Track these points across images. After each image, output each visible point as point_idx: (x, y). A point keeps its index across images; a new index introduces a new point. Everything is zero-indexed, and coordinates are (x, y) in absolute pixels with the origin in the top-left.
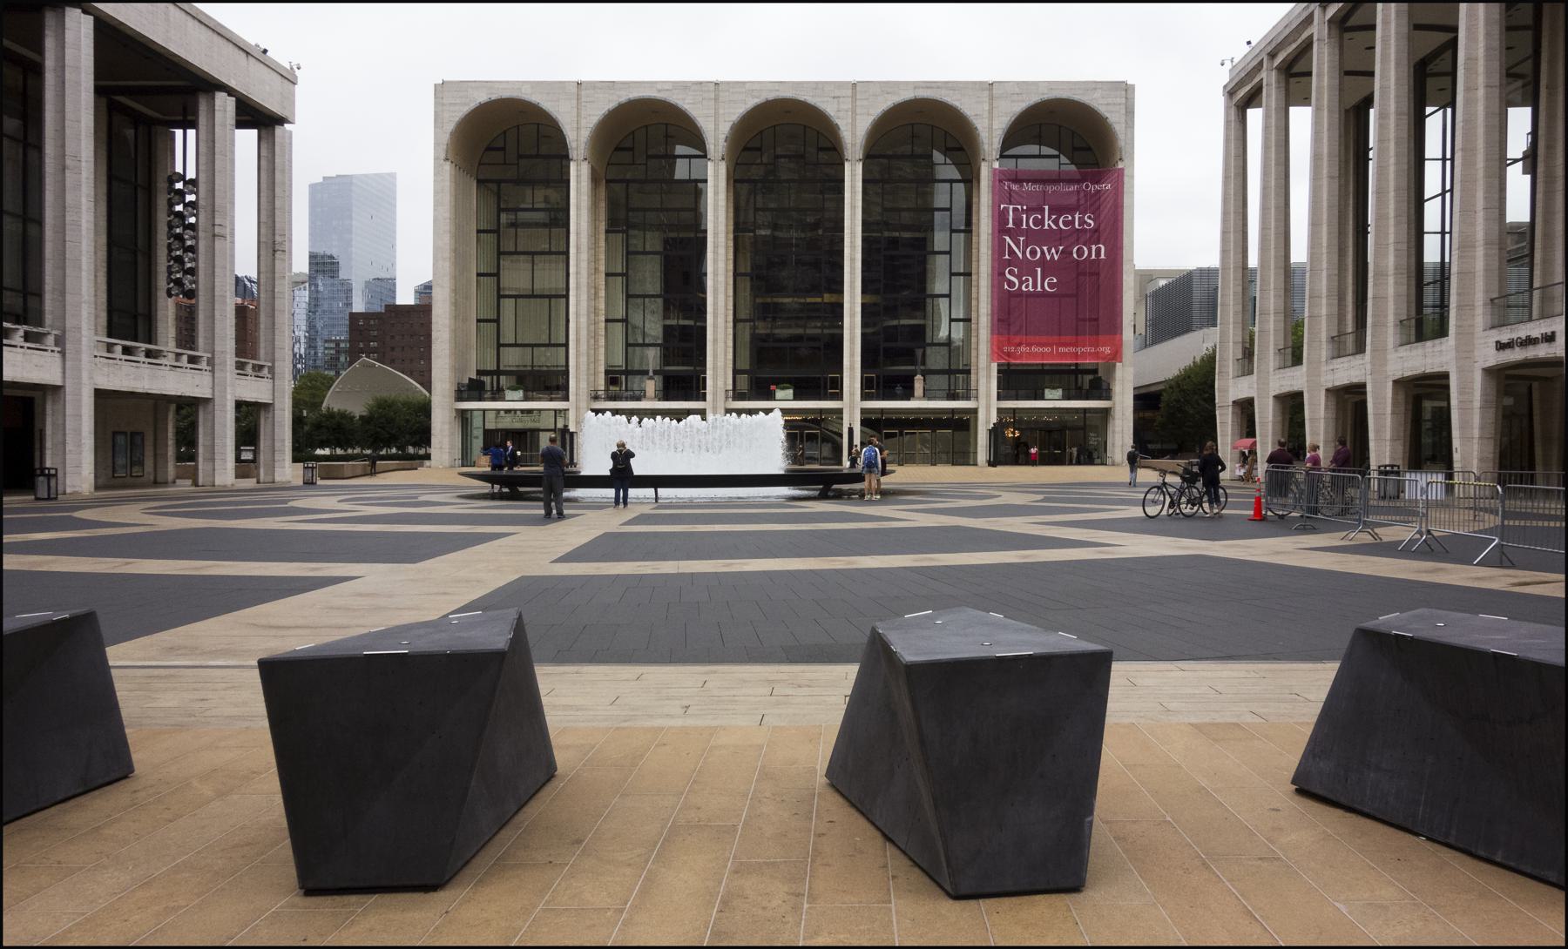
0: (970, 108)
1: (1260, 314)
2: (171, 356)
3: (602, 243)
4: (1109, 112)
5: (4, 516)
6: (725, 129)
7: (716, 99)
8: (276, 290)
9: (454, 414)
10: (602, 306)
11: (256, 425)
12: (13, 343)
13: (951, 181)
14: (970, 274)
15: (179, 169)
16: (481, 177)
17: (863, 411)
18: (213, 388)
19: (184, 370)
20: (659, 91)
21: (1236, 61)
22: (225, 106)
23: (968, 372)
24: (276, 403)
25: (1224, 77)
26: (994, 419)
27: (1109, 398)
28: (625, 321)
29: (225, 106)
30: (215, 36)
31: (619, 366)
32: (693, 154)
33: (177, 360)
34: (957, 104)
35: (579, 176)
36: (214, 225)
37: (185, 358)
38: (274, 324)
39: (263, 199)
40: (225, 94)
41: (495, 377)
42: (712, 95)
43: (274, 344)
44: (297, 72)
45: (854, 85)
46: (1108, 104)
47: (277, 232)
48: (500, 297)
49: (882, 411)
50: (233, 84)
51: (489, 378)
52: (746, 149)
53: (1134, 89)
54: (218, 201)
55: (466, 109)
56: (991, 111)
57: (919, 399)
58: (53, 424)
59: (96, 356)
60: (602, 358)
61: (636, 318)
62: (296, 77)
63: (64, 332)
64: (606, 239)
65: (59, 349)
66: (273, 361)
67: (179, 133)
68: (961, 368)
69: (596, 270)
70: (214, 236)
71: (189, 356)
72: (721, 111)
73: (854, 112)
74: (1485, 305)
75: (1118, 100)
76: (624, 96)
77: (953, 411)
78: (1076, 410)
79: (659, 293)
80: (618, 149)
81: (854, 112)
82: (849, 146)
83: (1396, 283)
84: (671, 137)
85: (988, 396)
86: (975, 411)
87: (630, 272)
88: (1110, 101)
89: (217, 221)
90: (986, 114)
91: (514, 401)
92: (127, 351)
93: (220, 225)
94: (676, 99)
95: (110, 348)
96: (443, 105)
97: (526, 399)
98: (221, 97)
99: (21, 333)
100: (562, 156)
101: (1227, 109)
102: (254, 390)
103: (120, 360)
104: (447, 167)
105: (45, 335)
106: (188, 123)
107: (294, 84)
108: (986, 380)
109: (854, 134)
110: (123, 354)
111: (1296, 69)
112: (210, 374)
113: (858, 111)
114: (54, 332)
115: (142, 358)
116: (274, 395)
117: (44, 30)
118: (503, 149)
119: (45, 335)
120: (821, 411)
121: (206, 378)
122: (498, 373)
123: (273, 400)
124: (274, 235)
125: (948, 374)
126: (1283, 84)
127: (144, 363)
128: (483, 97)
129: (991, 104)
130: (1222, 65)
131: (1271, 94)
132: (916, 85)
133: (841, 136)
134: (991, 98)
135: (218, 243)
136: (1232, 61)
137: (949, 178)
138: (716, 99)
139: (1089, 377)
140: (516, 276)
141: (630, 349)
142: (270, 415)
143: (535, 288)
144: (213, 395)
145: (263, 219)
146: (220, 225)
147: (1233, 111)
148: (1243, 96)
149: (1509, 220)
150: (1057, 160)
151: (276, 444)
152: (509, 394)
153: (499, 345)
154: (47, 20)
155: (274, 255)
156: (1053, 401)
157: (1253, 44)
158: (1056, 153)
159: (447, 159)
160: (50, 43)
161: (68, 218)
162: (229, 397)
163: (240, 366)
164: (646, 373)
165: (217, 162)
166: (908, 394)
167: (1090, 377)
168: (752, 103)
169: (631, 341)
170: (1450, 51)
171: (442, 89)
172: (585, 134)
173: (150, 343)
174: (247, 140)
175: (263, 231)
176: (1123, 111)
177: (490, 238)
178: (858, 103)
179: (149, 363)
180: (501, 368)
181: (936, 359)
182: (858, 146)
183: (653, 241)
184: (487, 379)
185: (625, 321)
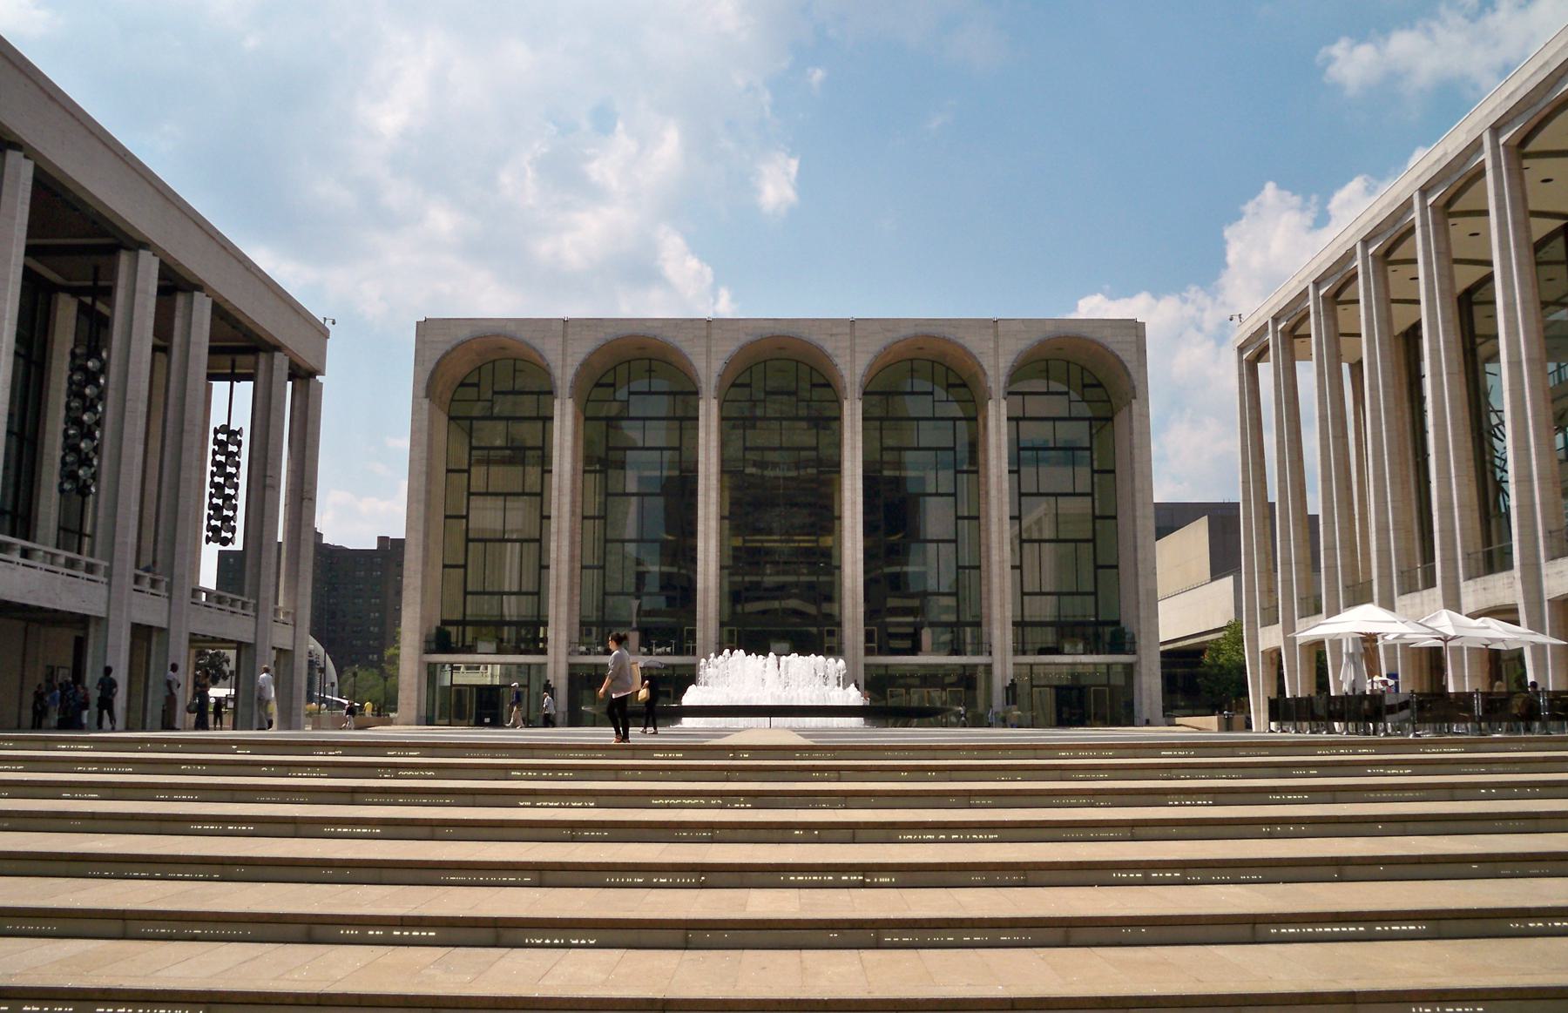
0: (977, 345)
5: (1467, 691)
6: (718, 366)
7: (708, 336)
8: (302, 538)
11: (1310, 645)
12: (47, 573)
13: (954, 419)
14: (978, 518)
16: (589, 414)
17: (867, 666)
18: (256, 634)
19: (238, 616)
22: (281, 363)
23: (978, 624)
24: (111, 618)
31: (589, 617)
36: (265, 476)
37: (239, 604)
41: (460, 628)
42: (704, 333)
44: (328, 324)
46: (1118, 342)
51: (455, 628)
52: (734, 385)
56: (996, 349)
58: (1263, 639)
62: (328, 331)
72: (713, 349)
73: (853, 351)
76: (610, 333)
80: (598, 385)
81: (853, 351)
82: (848, 385)
84: (521, 371)
85: (1004, 650)
88: (1120, 339)
89: (269, 473)
92: (71, 564)
93: (271, 476)
94: (816, 338)
98: (144, 255)
104: (426, 403)
108: (1001, 634)
110: (66, 567)
111: (1343, 297)
113: (857, 348)
115: (16, 557)
118: (477, 385)
121: (249, 624)
122: (463, 623)
125: (1026, 622)
129: (996, 343)
132: (917, 322)
134: (996, 335)
135: (305, 503)
137: (952, 415)
139: (1108, 630)
144: (256, 640)
146: (271, 476)
148: (1252, 355)
149: (252, 383)
150: (1067, 397)
152: (482, 646)
155: (301, 503)
158: (1065, 389)
164: (628, 624)
166: (915, 649)
167: (1113, 628)
168: (744, 339)
172: (570, 373)
173: (27, 539)
176: (1134, 349)
178: (857, 341)
180: (468, 618)
184: (452, 630)
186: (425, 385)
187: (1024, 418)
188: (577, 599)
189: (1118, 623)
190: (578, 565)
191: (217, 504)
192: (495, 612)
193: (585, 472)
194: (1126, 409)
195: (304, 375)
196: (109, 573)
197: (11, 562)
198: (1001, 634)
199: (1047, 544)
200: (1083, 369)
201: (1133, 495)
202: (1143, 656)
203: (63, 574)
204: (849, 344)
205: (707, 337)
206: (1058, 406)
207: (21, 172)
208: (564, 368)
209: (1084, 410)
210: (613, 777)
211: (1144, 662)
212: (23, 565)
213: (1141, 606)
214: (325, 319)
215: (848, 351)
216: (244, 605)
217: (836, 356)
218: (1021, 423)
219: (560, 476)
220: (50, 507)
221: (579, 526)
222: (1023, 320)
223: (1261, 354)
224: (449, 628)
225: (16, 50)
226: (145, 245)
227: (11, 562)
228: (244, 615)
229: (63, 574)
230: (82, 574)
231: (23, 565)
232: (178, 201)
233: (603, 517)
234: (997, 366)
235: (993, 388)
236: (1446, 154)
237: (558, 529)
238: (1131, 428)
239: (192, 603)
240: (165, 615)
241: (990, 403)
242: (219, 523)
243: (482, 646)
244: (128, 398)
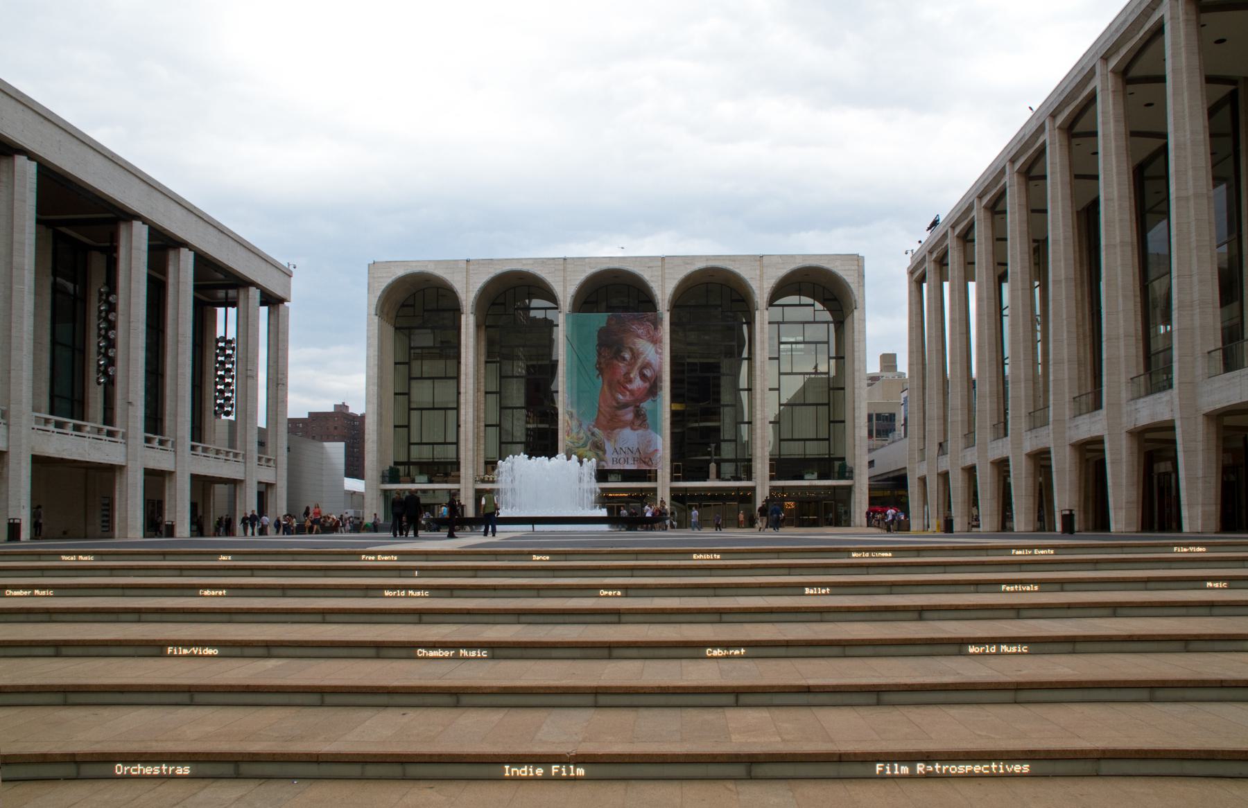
0: (746, 273)
1: (929, 420)
2: (214, 451)
3: (483, 371)
4: (847, 275)
6: (572, 289)
7: (564, 270)
9: (379, 493)
10: (482, 415)
13: (828, 323)
15: (220, 333)
16: (397, 325)
18: (245, 473)
20: (524, 265)
21: (914, 251)
22: (254, 294)
25: (907, 262)
26: (767, 493)
27: (851, 478)
28: (499, 425)
29: (254, 294)
30: (251, 254)
32: (548, 306)
33: (227, 456)
34: (737, 271)
35: (468, 323)
37: (231, 454)
38: (277, 431)
39: (271, 352)
40: (254, 288)
41: (407, 467)
42: (562, 267)
43: (277, 445)
44: (291, 268)
45: (663, 258)
46: (845, 270)
47: (279, 372)
48: (410, 409)
49: (686, 489)
50: (259, 281)
53: (864, 260)
54: (249, 355)
55: (389, 281)
57: (713, 480)
58: (169, 495)
59: (33, 429)
60: (482, 452)
61: (507, 425)
62: (291, 272)
63: (176, 439)
64: (485, 369)
65: (5, 422)
66: (276, 456)
67: (220, 311)
68: (746, 457)
69: (478, 390)
70: (247, 377)
71: (203, 448)
72: (568, 278)
74: (1026, 416)
75: (853, 268)
77: (739, 489)
78: (829, 487)
79: (523, 406)
80: (493, 304)
82: (660, 301)
83: (990, 402)
86: (753, 489)
87: (503, 390)
88: (847, 268)
90: (758, 278)
91: (421, 485)
92: (59, 425)
93: (250, 370)
94: (440, 272)
95: (148, 440)
96: (374, 278)
97: (430, 481)
98: (137, 225)
99: (157, 440)
100: (456, 310)
101: (910, 283)
102: (267, 475)
103: (53, 432)
104: (376, 319)
105: (167, 441)
106: (227, 303)
107: (290, 276)
108: (761, 468)
109: (663, 293)
110: (74, 430)
112: (173, 453)
113: (667, 276)
114: (171, 439)
116: (276, 479)
117: (168, 262)
118: (413, 306)
119: (167, 441)
120: (641, 489)
122: (408, 463)
123: (276, 481)
124: (277, 373)
126: (938, 271)
127: (72, 435)
128: (401, 272)
130: (906, 253)
131: (931, 276)
132: (707, 258)
133: (654, 293)
134: (762, 266)
136: (912, 251)
138: (564, 270)
140: (422, 393)
141: (503, 446)
142: (274, 491)
143: (436, 400)
144: (245, 477)
145: (271, 363)
147: (914, 285)
148: (918, 279)
151: (278, 510)
152: (418, 478)
153: (410, 444)
154: (121, 229)
155: (277, 387)
156: (810, 481)
157: (923, 242)
159: (376, 315)
160: (171, 269)
161: (179, 371)
162: (254, 479)
163: (193, 448)
165: (250, 331)
166: (706, 477)
167: (840, 462)
168: (589, 271)
169: (503, 440)
170: (1166, 201)
171: (374, 267)
174: (264, 310)
175: (270, 371)
176: (856, 275)
177: (403, 368)
179: (76, 435)
181: (727, 451)
182: (667, 301)
183: (520, 368)
184: (401, 468)
185: (499, 425)
186: (375, 306)
187: (783, 323)
188: (482, 447)
189: (843, 459)
190: (482, 424)
191: (221, 389)
192: (801, 452)
193: (486, 362)
194: (851, 315)
195: (272, 301)
196: (244, 456)
197: (48, 431)
198: (761, 468)
199: (415, 411)
200: (824, 288)
201: (854, 373)
202: (857, 481)
203: (89, 438)
204: (660, 273)
205: (564, 270)
206: (807, 313)
207: (26, 171)
208: (468, 293)
209: (827, 316)
210: (494, 559)
211: (857, 485)
212: (58, 433)
213: (856, 447)
214: (289, 265)
215: (660, 278)
216: (236, 455)
217: (652, 281)
218: (781, 325)
219: (466, 365)
220: (97, 394)
221: (482, 399)
222: (781, 256)
223: (922, 279)
224: (399, 467)
225: (11, 86)
226: (184, 244)
227: (48, 431)
228: (235, 461)
229: (89, 438)
230: (104, 437)
231: (58, 433)
232: (159, 186)
233: (499, 393)
234: (761, 288)
235: (759, 303)
236: (1024, 135)
237: (466, 400)
238: (853, 328)
239: (193, 454)
240: (173, 462)
241: (757, 312)
242: (222, 401)
243: (807, 477)
244: (131, 320)
